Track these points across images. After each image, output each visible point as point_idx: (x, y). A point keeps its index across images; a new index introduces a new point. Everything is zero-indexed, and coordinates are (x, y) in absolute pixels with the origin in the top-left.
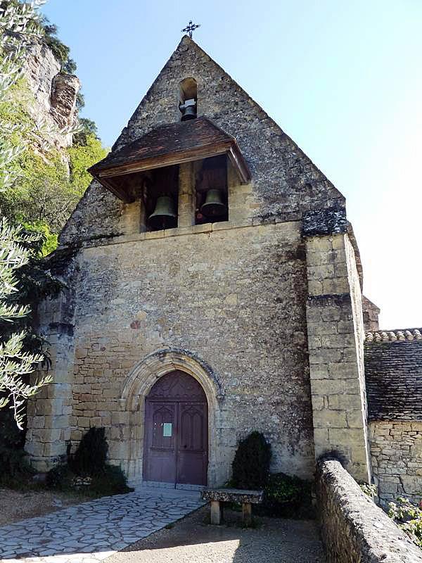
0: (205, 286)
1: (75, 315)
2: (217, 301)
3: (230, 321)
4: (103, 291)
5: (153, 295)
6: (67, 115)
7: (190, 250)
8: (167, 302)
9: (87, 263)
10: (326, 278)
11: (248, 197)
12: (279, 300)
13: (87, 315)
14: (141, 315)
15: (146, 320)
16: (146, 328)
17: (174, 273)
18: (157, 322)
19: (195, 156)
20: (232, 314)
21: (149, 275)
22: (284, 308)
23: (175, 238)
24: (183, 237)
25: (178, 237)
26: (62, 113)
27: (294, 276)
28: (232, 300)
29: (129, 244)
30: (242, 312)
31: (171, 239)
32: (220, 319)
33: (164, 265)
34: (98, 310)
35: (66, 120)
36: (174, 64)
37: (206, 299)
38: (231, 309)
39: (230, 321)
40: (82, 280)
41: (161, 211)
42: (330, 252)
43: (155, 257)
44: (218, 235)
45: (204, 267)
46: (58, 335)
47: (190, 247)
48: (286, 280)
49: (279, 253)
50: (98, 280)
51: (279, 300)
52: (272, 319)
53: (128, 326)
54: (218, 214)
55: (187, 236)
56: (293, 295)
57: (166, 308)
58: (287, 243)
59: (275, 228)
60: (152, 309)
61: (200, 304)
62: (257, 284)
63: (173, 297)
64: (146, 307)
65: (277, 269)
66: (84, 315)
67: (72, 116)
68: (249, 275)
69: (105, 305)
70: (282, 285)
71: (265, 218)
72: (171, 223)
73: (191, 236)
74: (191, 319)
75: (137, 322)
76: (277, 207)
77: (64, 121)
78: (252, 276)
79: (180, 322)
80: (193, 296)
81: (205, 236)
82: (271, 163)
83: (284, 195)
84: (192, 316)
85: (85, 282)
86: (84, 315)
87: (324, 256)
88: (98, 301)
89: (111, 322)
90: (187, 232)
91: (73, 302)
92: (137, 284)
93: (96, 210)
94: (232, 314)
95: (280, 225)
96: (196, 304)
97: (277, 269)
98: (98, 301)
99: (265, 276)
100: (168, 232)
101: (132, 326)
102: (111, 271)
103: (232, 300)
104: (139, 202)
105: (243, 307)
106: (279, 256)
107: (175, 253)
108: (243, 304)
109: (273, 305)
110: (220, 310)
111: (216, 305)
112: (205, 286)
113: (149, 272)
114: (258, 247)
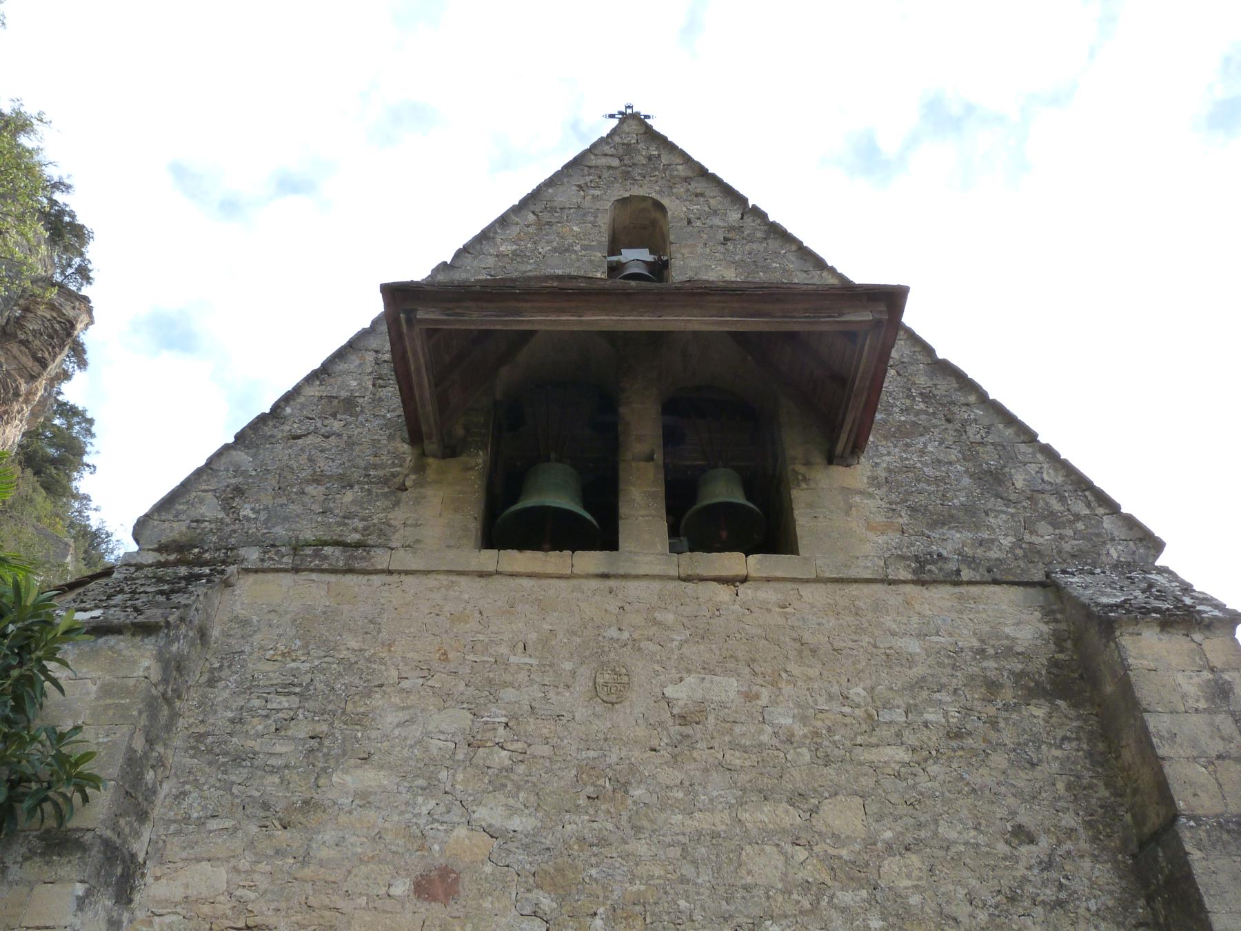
0: (735, 759)
1: (155, 814)
2: (790, 817)
3: (845, 897)
4: (301, 730)
5: (521, 769)
6: (33, 378)
7: (667, 628)
8: (582, 801)
9: (245, 623)
10: (1219, 757)
11: (857, 499)
12: (1022, 835)
13: (213, 825)
14: (459, 843)
15: (488, 868)
16: (487, 904)
17: (611, 691)
18: (539, 880)
19: (769, 315)
20: (856, 872)
21: (509, 694)
22: (1047, 865)
23: (611, 583)
24: (643, 584)
25: (623, 583)
26: (22, 370)
27: (1058, 753)
28: (843, 818)
29: (431, 581)
30: (891, 865)
31: (595, 584)
32: (806, 886)
33: (568, 666)
34: (266, 806)
35: (23, 388)
36: (593, 161)
37: (741, 803)
38: (844, 853)
39: (845, 897)
40: (212, 683)
41: (555, 494)
42: (1207, 675)
43: (533, 636)
44: (769, 594)
45: (728, 688)
46: (80, 889)
47: (669, 618)
48: (1033, 765)
49: (991, 674)
50: (285, 689)
51: (1022, 835)
52: (1012, 899)
53: (401, 888)
54: (765, 528)
55: (656, 585)
56: (1069, 820)
57: (576, 825)
58: (1010, 649)
59: (960, 598)
60: (516, 823)
61: (720, 820)
62: (933, 769)
63: (606, 786)
64: (490, 813)
65: (993, 723)
66: (201, 823)
67: (42, 383)
68: (899, 735)
69: (302, 790)
70: (1022, 779)
71: (927, 570)
72: (596, 530)
73: (672, 585)
74: (683, 880)
75: (445, 872)
76: (952, 541)
77: (17, 389)
78: (911, 739)
79: (639, 886)
80: (690, 787)
81: (723, 593)
82: (914, 424)
83: (968, 509)
84: (688, 870)
85: (221, 694)
86: (201, 823)
87: (1191, 685)
88: (274, 770)
89: (321, 864)
90: (657, 570)
91: (160, 763)
92: (456, 720)
93: (310, 460)
94: (856, 872)
95: (974, 590)
96: (702, 821)
97: (993, 723)
98: (274, 770)
99: (954, 744)
100: (589, 561)
101: (423, 889)
102: (349, 666)
103: (843, 818)
104: (480, 459)
105: (889, 848)
106: (993, 686)
107: (613, 632)
108: (888, 835)
109: (1002, 848)
110: (801, 854)
111: (784, 831)
112: (735, 759)
113: (506, 685)
114: (914, 646)
